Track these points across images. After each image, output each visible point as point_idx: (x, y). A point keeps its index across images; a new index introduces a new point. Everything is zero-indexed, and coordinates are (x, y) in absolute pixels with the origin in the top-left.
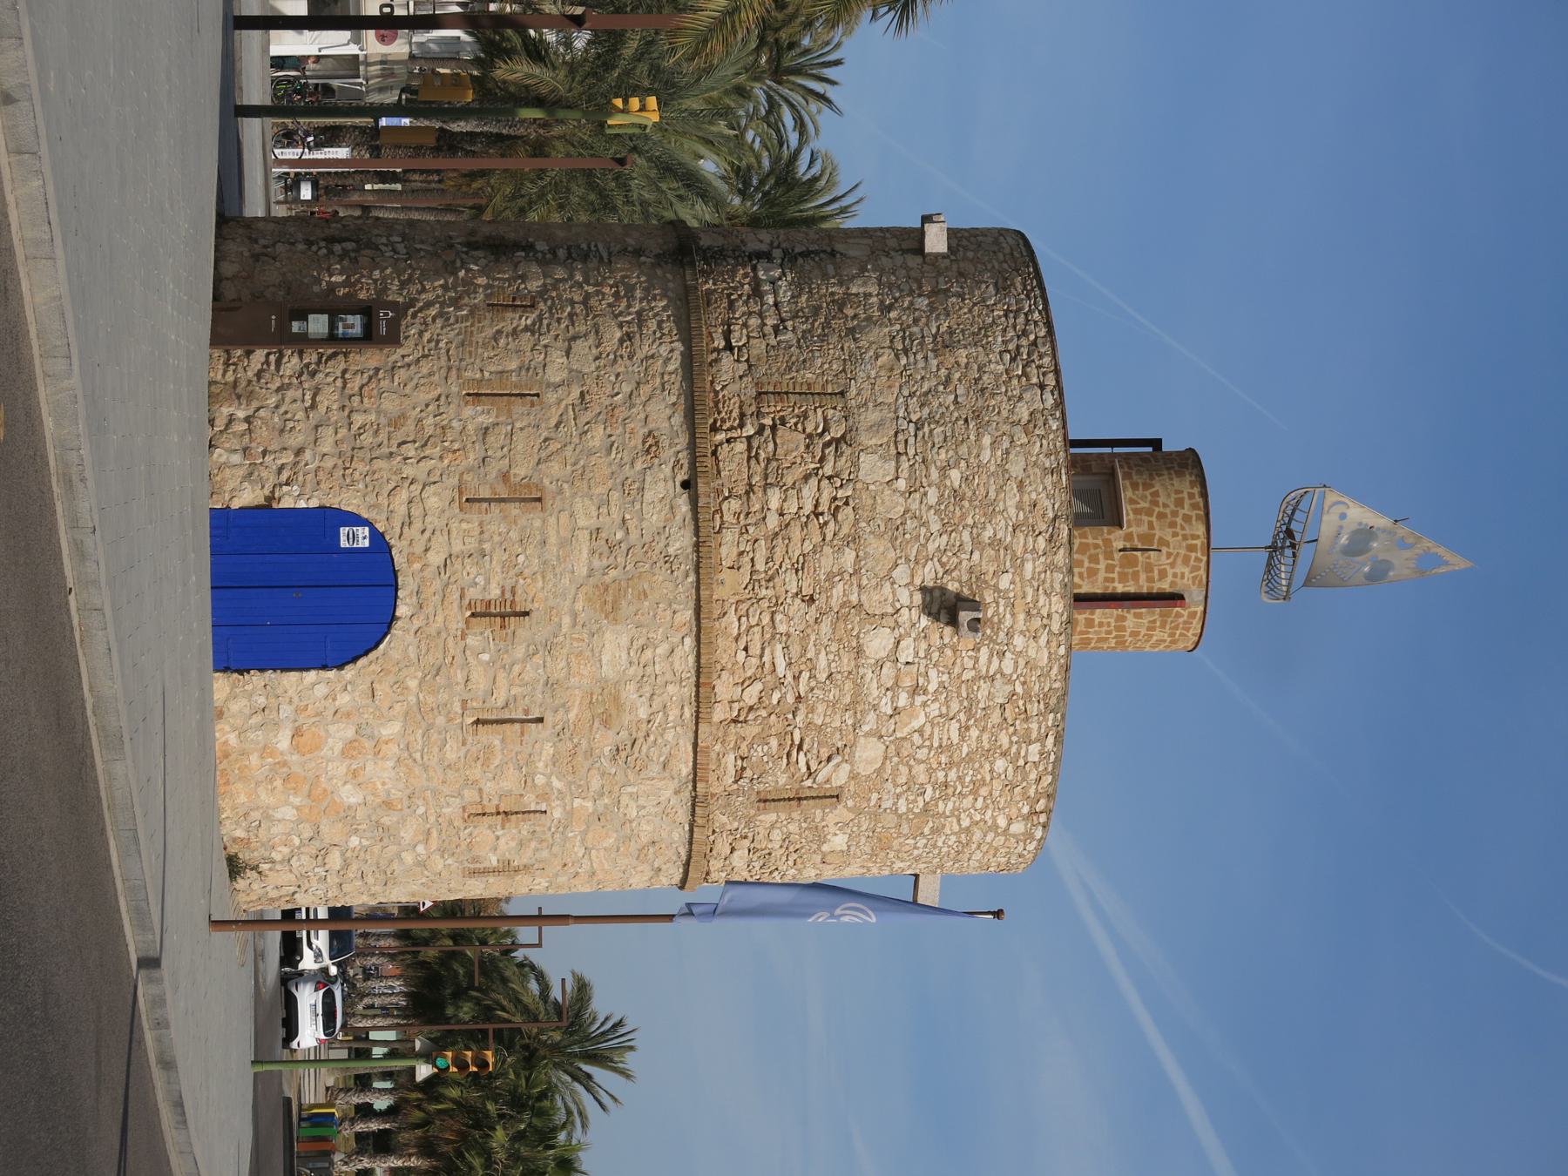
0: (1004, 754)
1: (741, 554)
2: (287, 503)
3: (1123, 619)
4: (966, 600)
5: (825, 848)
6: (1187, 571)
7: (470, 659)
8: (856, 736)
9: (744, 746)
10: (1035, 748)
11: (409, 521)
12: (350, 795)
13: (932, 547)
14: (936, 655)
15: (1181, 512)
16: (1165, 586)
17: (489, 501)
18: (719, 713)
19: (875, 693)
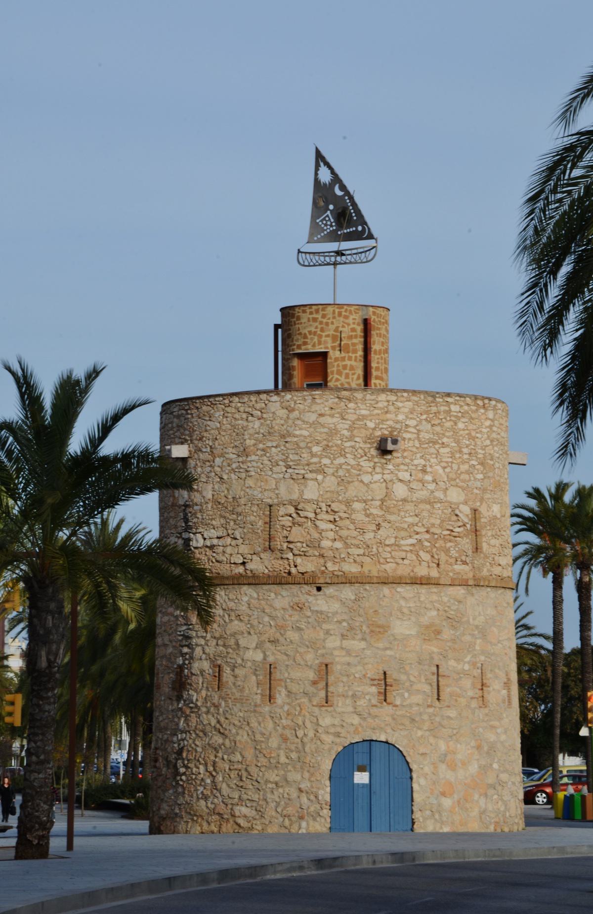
0: (456, 424)
1: (355, 561)
3: (375, 350)
5: (499, 516)
6: (351, 317)
8: (446, 502)
11: (338, 735)
12: (473, 768)
13: (352, 462)
14: (407, 461)
15: (320, 319)
16: (359, 329)
17: (327, 692)
18: (434, 573)
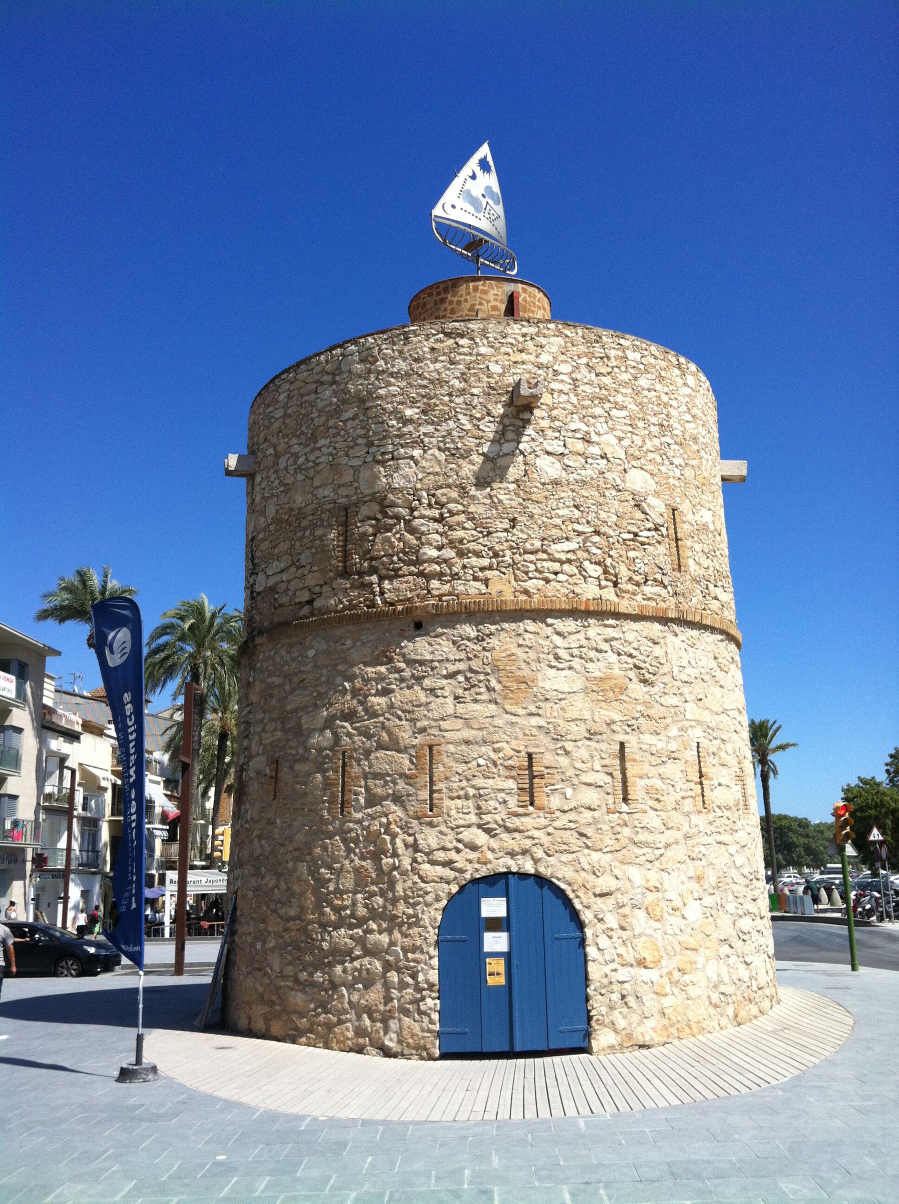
0: (636, 379)
2: (434, 976)
4: (512, 398)
6: (492, 292)
7: (572, 806)
9: (637, 578)
10: (629, 353)
14: (557, 423)
19: (589, 472)
